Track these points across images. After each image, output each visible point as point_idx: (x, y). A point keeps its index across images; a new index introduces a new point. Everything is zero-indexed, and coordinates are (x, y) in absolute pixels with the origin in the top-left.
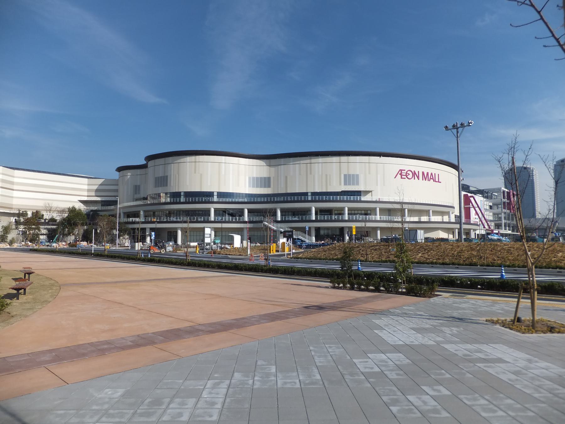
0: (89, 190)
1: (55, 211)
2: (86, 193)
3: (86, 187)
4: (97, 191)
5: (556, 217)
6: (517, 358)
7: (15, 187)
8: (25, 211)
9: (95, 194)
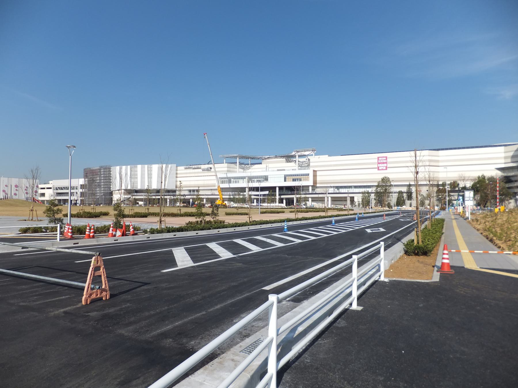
0: (505, 158)
1: (468, 180)
2: (503, 161)
3: (503, 155)
4: (513, 157)
5: (112, 168)
6: (48, 188)
7: (440, 164)
8: (445, 182)
9: (511, 160)
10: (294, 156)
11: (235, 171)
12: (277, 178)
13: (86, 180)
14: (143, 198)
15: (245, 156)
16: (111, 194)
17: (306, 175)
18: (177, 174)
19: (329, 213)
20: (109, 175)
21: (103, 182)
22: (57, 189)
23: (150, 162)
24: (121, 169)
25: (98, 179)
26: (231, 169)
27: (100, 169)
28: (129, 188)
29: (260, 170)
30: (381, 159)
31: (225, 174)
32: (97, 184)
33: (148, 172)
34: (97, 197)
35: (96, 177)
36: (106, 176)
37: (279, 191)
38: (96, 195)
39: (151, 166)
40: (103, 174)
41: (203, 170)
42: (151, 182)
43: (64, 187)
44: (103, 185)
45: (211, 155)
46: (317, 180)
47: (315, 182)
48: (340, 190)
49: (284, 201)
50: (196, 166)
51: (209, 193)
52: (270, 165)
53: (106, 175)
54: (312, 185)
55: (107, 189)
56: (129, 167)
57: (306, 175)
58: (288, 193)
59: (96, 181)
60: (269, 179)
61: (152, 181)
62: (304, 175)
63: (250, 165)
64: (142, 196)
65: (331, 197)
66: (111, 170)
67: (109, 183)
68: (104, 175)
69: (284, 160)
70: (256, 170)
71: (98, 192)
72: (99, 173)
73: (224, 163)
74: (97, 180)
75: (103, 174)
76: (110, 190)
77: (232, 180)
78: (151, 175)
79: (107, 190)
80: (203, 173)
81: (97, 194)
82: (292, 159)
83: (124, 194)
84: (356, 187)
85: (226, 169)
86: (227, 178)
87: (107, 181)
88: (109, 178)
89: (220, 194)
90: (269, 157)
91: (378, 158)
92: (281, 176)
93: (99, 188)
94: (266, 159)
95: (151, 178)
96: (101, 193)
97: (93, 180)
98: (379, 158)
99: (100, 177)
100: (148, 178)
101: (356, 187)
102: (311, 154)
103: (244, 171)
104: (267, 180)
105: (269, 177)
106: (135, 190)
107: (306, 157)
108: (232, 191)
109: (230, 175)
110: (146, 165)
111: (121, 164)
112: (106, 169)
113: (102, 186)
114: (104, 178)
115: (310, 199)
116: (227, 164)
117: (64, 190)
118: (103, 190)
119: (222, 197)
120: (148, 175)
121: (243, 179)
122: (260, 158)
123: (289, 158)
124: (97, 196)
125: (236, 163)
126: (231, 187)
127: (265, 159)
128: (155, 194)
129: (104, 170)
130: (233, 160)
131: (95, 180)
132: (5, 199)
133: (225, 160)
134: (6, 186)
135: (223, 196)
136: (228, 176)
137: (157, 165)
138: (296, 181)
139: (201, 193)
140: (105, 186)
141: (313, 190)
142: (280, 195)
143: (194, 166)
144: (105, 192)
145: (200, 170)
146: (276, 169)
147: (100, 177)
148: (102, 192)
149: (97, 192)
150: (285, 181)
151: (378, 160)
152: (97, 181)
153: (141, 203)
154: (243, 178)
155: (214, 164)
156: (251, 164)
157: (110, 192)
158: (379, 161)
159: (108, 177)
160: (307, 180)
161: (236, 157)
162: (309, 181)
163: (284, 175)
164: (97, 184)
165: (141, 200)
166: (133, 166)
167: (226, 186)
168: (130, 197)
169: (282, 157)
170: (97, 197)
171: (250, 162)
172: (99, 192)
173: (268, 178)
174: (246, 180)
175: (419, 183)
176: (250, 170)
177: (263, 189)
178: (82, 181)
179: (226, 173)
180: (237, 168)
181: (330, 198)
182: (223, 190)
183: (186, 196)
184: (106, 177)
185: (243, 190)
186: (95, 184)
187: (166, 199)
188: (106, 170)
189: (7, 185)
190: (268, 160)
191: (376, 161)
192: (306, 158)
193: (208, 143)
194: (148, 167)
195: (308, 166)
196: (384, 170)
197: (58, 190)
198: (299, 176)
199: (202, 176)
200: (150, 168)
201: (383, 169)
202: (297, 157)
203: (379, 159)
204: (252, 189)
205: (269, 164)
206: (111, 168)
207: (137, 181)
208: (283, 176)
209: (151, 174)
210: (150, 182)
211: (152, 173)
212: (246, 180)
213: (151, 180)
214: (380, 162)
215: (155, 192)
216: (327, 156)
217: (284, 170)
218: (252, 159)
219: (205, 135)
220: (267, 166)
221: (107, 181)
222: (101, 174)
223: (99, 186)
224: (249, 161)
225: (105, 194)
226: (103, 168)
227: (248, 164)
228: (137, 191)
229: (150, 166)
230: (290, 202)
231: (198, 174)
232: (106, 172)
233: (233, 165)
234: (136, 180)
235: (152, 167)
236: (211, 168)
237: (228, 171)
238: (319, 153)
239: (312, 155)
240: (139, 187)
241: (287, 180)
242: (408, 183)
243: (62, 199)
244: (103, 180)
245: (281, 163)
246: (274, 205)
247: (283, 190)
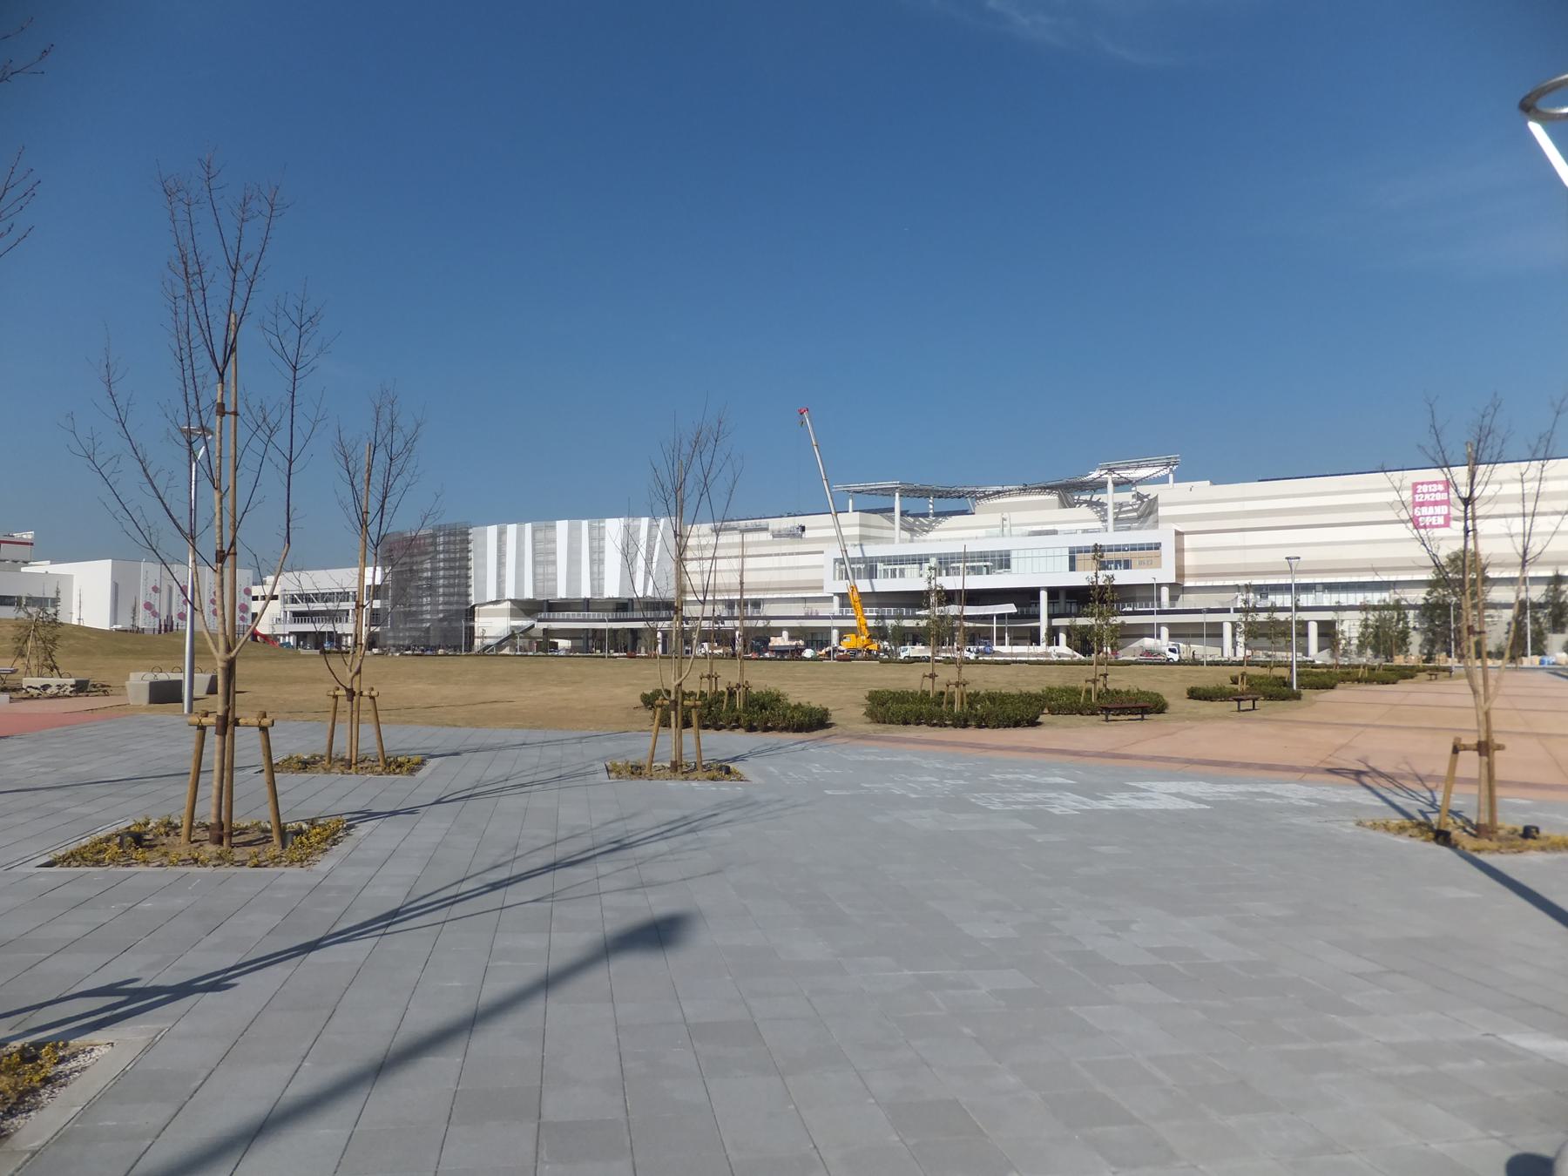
10: (1100, 486)
11: (883, 538)
12: (1027, 559)
15: (921, 487)
16: (470, 614)
17: (1150, 549)
19: (199, 656)
20: (463, 555)
21: (444, 577)
22: (294, 601)
23: (599, 512)
24: (501, 534)
25: (429, 566)
26: (873, 532)
27: (434, 536)
28: (528, 594)
29: (982, 532)
30: (1425, 488)
31: (858, 547)
32: (424, 583)
33: (590, 543)
34: (424, 625)
35: (422, 562)
36: (452, 556)
37: (1048, 603)
38: (420, 617)
39: (601, 525)
40: (443, 551)
41: (778, 535)
42: (601, 576)
43: (317, 594)
44: (444, 586)
45: (825, 482)
46: (1183, 566)
47: (1180, 573)
48: (1271, 597)
49: (1063, 637)
50: (750, 523)
51: (798, 610)
52: (1016, 517)
53: (455, 553)
54: (1174, 581)
55: (456, 598)
56: (528, 527)
57: (1149, 549)
58: (1068, 609)
59: (420, 575)
60: (1013, 563)
61: (603, 573)
62: (1086, 552)
63: (932, 519)
65: (1317, 621)
66: (470, 537)
67: (463, 581)
68: (447, 556)
69: (1054, 498)
70: (951, 535)
71: (429, 608)
72: (431, 549)
73: (848, 512)
74: (423, 571)
75: (443, 551)
76: (468, 603)
77: (880, 566)
78: (599, 552)
79: (457, 603)
80: (779, 544)
81: (422, 615)
82: (1076, 497)
83: (513, 614)
84: (1330, 587)
86: (864, 560)
87: (457, 572)
88: (463, 563)
89: (860, 613)
90: (1000, 488)
91: (1415, 485)
92: (1058, 552)
93: (430, 595)
94: (990, 495)
95: (601, 562)
96: (438, 612)
97: (411, 570)
98: (1419, 487)
99: (433, 559)
100: (592, 561)
101: (1330, 587)
102: (1155, 476)
103: (912, 536)
104: (1008, 566)
105: (1013, 555)
106: (548, 601)
107: (1134, 489)
108: (880, 605)
109: (872, 551)
110: (584, 519)
111: (502, 519)
112: (455, 535)
113: (441, 590)
114: (447, 564)
115: (1165, 631)
116: (858, 513)
117: (317, 604)
118: (445, 603)
119: (866, 624)
120: (592, 551)
121: (921, 564)
122: (969, 492)
123: (1070, 491)
124: (422, 621)
125: (892, 510)
126: (877, 590)
127: (987, 496)
128: (611, 615)
129: (447, 539)
130: (881, 502)
131: (417, 571)
132: (163, 632)
133: (850, 501)
134: (155, 589)
135: (868, 621)
136: (867, 555)
137: (515, 525)
138: (981, 574)
139: (768, 610)
140: (452, 590)
141: (1173, 598)
142: (1051, 616)
143: (742, 523)
144: (451, 607)
145: (765, 536)
147: (433, 559)
148: (441, 607)
149: (424, 608)
150: (1072, 568)
151: (1415, 492)
152: (425, 575)
153: (564, 644)
154: (919, 560)
155: (837, 513)
156: (937, 515)
157: (467, 610)
158: (1417, 496)
159: (461, 559)
160: (1156, 563)
161: (889, 493)
162: (1160, 567)
163: (1070, 548)
164: (424, 583)
165: (564, 634)
166: (542, 524)
168: (533, 626)
169: (1045, 488)
170: (424, 625)
171: (931, 506)
172: (431, 610)
173: (1009, 560)
175: (1187, 584)
176: (932, 535)
179: (861, 545)
180: (894, 529)
181: (1316, 624)
183: (725, 622)
184: (454, 560)
186: (420, 583)
187: (1304, 624)
188: (452, 538)
189: (158, 587)
190: (998, 501)
192: (1131, 491)
193: (814, 443)
194: (591, 528)
195: (1139, 517)
196: (1437, 526)
197: (296, 602)
198: (1124, 550)
199: (771, 555)
200: (597, 531)
201: (1434, 523)
202: (1110, 486)
203: (1419, 491)
205: (1011, 513)
206: (470, 531)
207: (555, 574)
208: (1066, 552)
210: (597, 578)
211: (603, 547)
213: (502, 573)
214: (1421, 500)
215: (611, 607)
217: (1055, 532)
218: (940, 497)
219: (802, 414)
220: (1004, 519)
221: (457, 572)
222: (439, 553)
223: (432, 589)
224: (931, 505)
225: (450, 616)
226: (444, 530)
227: (926, 515)
228: (553, 607)
229: (597, 524)
230: (1084, 642)
231: (758, 548)
232: (454, 543)
233: (876, 519)
234: (550, 569)
235: (604, 527)
236: (803, 529)
238: (1184, 475)
239: (1164, 480)
240: (562, 594)
241: (1078, 564)
242: (1549, 573)
243: (1206, 623)
244: (444, 569)
245: (1042, 510)
246: (1033, 649)
247: (1058, 598)
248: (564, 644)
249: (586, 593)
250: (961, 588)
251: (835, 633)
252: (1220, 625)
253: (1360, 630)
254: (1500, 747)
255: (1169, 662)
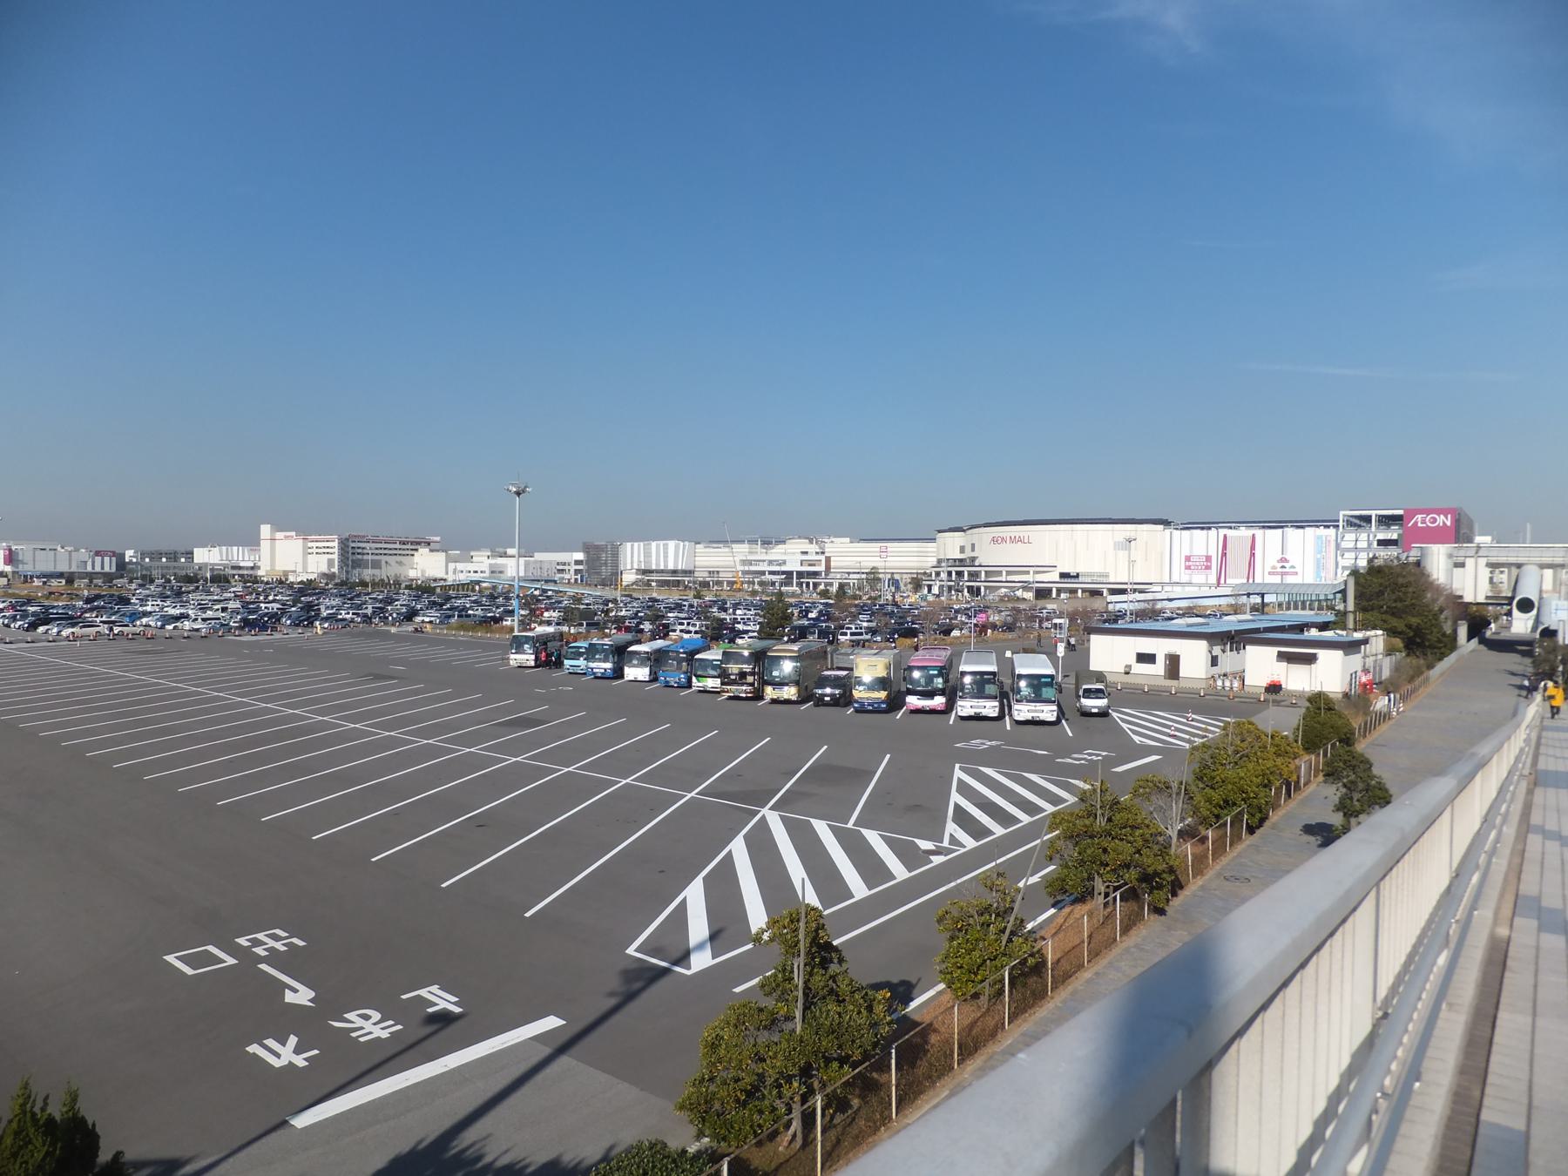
13: (1344, 545)
14: (1536, 708)
18: (695, 552)
24: (632, 546)
26: (754, 550)
64: (655, 577)
70: (777, 552)
85: (747, 550)
99: (606, 553)
120: (664, 553)
141: (986, 576)
146: (800, 551)
147: (606, 553)
160: (820, 565)
167: (747, 568)
174: (766, 563)
177: (783, 573)
178: (580, 556)
182: (745, 573)
185: (763, 573)
191: (878, 549)
204: (772, 573)
209: (667, 553)
210: (666, 562)
212: (766, 563)
216: (848, 540)
223: (606, 564)
228: (651, 572)
233: (755, 546)
237: (749, 552)
240: (654, 567)
248: (654, 584)
249: (662, 568)
250: (514, 574)
251: (983, 573)
252: (1371, 516)
253: (703, 1149)
254: (1238, 653)
255: (673, 687)
